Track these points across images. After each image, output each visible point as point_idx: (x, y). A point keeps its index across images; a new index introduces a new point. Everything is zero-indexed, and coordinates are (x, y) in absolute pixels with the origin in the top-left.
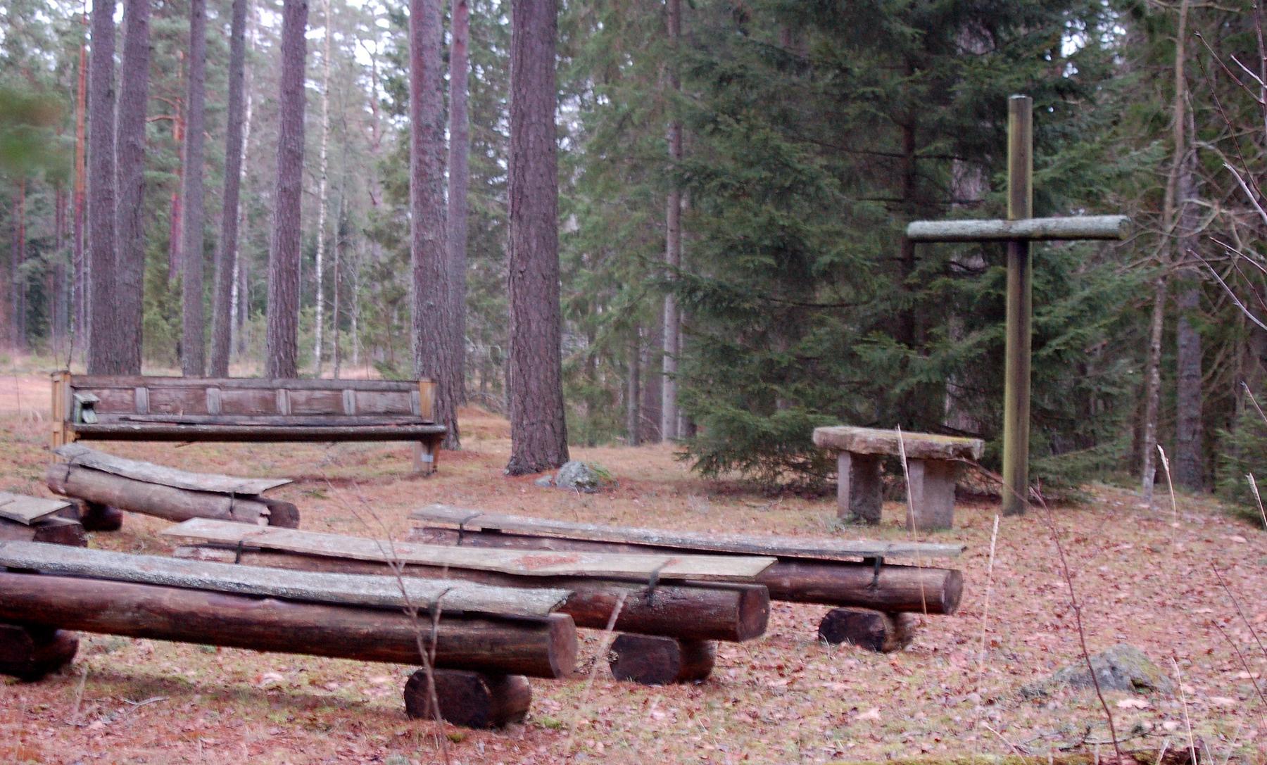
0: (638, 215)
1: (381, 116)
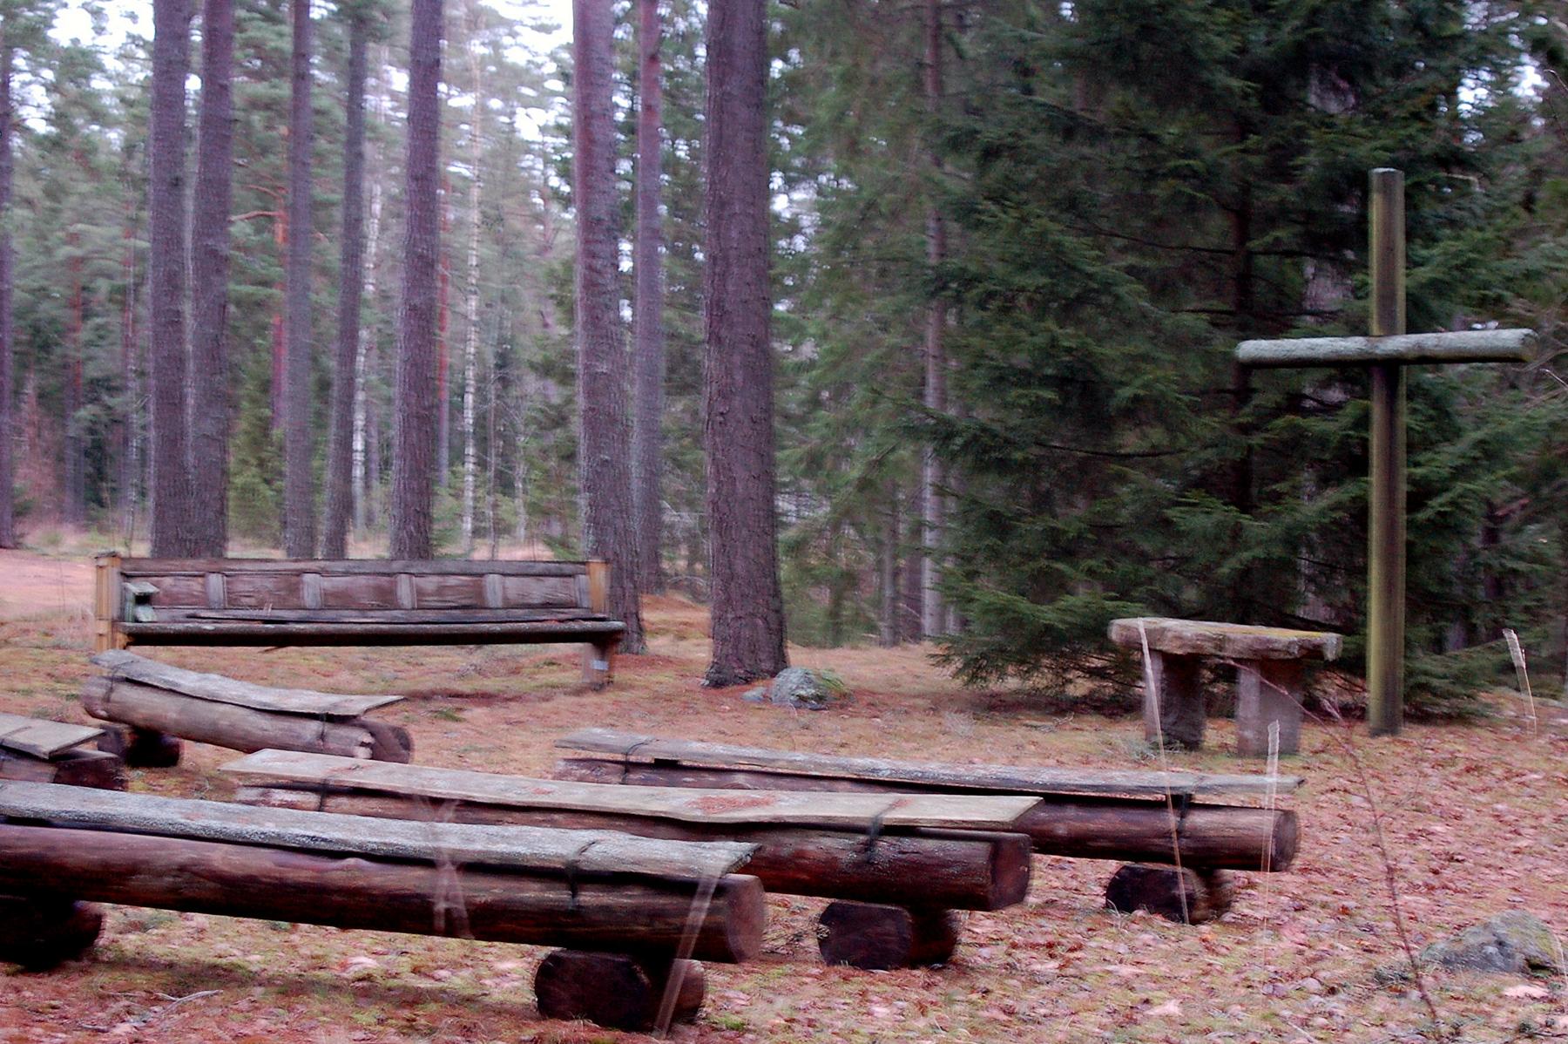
0: (891, 339)
1: (555, 208)
